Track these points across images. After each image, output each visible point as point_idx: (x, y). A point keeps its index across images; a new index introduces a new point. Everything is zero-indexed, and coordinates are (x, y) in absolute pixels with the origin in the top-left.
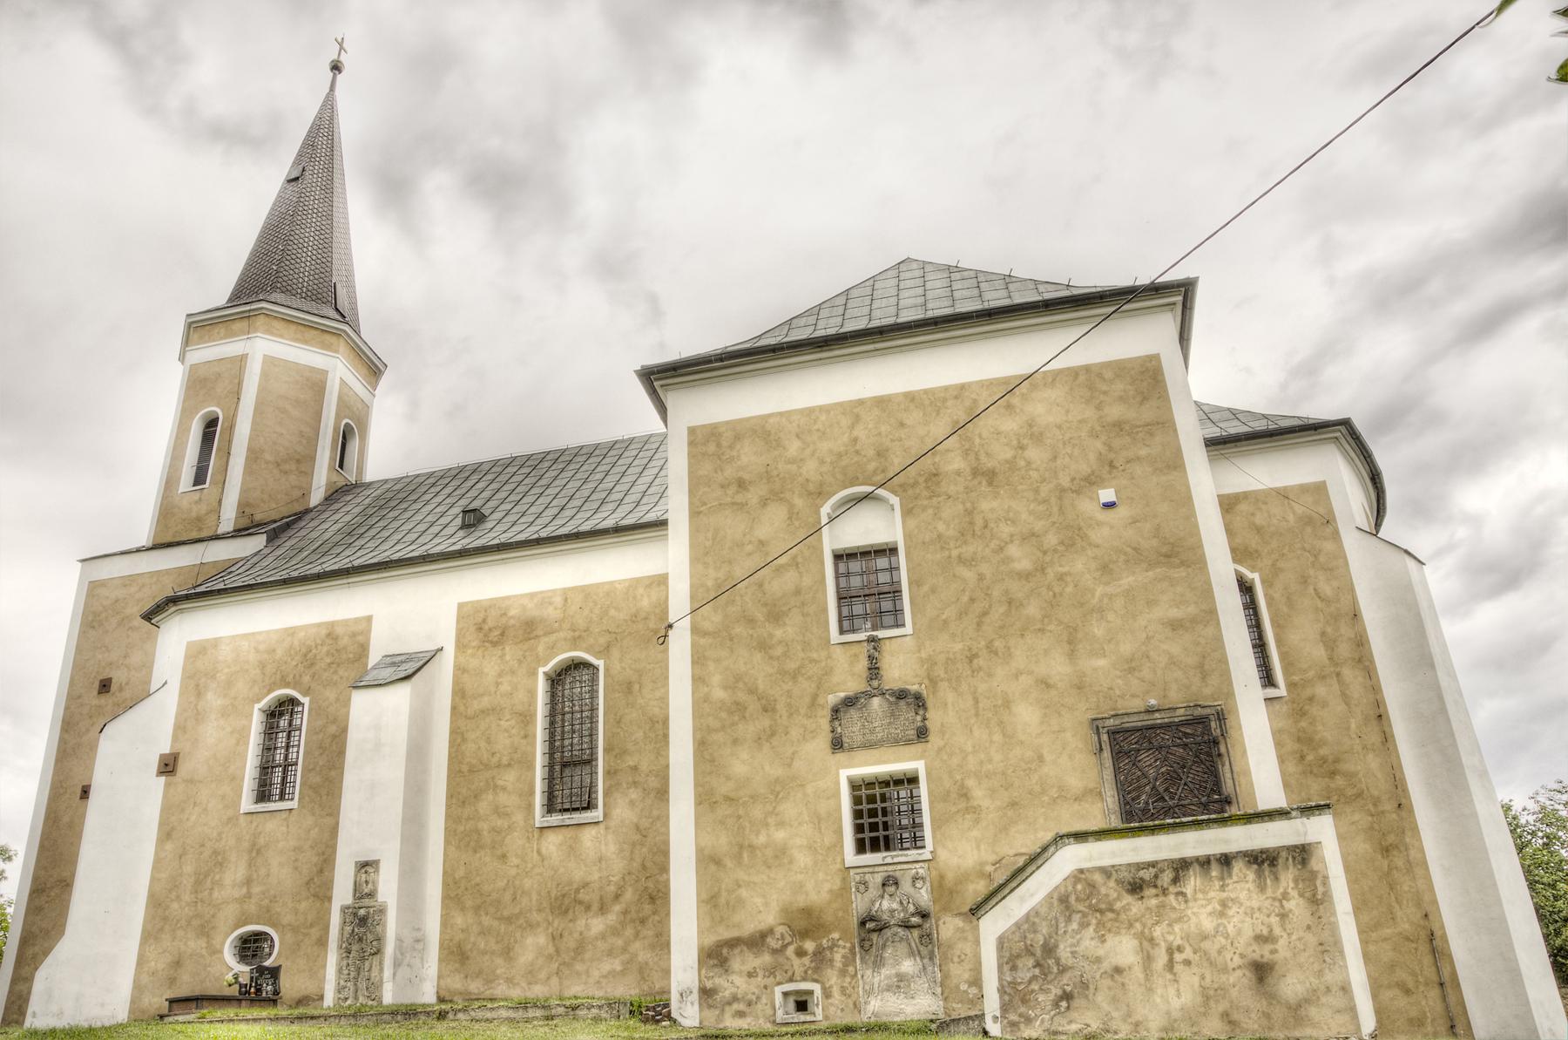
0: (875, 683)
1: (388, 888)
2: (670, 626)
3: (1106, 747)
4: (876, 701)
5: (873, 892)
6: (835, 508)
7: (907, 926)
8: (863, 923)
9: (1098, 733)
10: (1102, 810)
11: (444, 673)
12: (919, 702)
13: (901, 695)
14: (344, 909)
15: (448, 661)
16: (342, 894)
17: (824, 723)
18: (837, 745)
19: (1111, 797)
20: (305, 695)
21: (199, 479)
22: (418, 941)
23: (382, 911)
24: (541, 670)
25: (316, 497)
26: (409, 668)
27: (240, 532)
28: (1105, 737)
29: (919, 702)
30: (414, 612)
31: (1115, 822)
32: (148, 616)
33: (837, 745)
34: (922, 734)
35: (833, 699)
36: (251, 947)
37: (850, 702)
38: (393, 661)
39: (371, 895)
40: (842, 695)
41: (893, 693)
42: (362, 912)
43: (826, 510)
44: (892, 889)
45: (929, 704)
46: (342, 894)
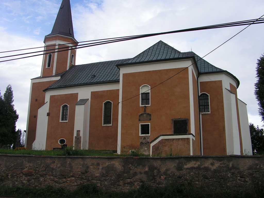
0: (145, 112)
1: (81, 134)
2: (119, 103)
3: (173, 123)
4: (145, 115)
5: (142, 139)
6: (142, 87)
7: (146, 144)
8: (141, 143)
9: (172, 121)
10: (172, 132)
11: (89, 102)
12: (150, 115)
13: (148, 114)
14: (75, 137)
15: (90, 99)
16: (75, 135)
17: (138, 117)
18: (139, 120)
19: (173, 129)
20: (68, 105)
21: (49, 66)
22: (86, 142)
23: (81, 137)
24: (103, 103)
25: (68, 69)
26: (83, 102)
27: (56, 76)
28: (173, 122)
29: (150, 115)
30: (84, 93)
31: (173, 134)
32: (44, 91)
33: (139, 120)
34: (150, 119)
35: (139, 114)
36: (62, 141)
37: (142, 115)
38: (82, 100)
39: (79, 135)
40: (141, 114)
41: (147, 113)
42: (78, 137)
43: (140, 87)
44: (145, 139)
45: (152, 115)
46: (75, 135)
